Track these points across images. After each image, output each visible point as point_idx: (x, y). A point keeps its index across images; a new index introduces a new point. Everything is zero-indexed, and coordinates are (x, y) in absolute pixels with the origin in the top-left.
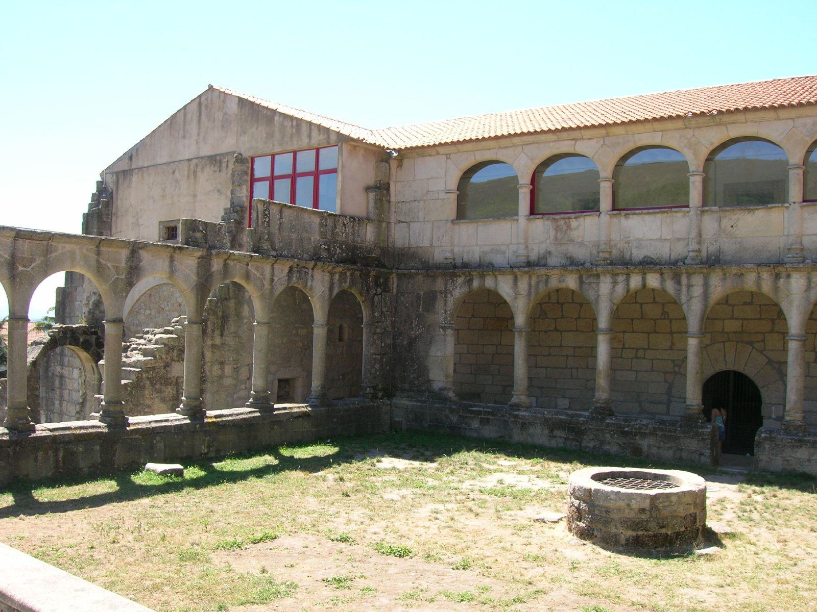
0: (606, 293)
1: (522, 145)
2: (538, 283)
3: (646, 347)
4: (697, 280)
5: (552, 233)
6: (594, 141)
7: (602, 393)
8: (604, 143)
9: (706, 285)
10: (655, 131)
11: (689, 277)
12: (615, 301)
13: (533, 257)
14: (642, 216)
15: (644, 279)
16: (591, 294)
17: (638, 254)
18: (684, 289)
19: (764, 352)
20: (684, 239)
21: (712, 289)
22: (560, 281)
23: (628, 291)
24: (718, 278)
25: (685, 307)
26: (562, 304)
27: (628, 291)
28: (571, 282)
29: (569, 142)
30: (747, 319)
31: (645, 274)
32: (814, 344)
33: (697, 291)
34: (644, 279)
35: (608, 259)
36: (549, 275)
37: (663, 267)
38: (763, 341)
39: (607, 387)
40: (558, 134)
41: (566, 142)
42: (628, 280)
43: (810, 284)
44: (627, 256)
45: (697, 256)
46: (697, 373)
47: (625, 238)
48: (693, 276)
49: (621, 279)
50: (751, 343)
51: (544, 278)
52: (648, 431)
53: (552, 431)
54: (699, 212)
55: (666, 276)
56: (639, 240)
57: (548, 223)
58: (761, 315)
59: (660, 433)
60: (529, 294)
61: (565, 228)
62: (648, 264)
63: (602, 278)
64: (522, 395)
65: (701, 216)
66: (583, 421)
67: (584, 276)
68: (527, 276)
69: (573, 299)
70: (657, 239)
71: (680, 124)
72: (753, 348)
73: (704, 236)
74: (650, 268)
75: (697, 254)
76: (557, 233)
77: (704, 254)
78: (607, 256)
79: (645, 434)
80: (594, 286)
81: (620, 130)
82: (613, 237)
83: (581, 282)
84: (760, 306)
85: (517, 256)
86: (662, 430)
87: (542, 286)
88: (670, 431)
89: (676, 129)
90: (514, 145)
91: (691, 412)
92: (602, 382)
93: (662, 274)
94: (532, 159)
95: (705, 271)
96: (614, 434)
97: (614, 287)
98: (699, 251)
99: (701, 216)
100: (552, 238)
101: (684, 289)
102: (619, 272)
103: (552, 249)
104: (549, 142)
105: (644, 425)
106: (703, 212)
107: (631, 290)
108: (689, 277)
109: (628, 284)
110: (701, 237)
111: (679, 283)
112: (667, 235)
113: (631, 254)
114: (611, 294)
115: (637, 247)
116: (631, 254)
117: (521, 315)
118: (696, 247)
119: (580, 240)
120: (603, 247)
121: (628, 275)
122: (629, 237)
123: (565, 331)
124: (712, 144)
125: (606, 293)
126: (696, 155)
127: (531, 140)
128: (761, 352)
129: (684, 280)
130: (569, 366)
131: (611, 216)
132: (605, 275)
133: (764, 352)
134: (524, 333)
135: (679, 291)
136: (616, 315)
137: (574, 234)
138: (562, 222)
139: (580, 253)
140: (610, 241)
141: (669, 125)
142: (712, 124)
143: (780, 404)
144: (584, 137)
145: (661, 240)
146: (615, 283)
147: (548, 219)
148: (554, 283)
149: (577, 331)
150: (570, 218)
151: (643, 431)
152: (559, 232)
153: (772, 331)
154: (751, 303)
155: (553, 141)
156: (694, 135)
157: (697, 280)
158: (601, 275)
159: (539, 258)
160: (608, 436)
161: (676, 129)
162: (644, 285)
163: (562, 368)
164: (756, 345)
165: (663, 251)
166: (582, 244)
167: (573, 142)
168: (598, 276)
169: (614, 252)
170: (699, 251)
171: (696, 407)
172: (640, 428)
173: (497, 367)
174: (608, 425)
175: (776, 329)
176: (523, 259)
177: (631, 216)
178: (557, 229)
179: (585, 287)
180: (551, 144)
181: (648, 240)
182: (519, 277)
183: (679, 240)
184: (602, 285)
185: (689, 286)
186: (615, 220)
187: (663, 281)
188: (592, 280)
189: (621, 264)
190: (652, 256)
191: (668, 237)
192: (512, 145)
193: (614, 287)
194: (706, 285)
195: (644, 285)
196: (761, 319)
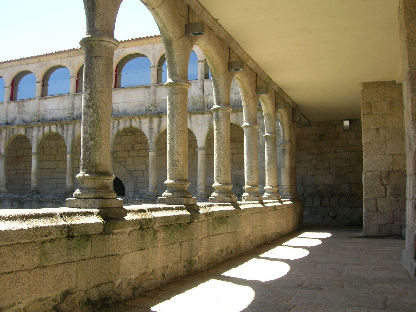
0: (36, 136)
1: (7, 68)
2: (9, 132)
3: (77, 167)
4: (70, 127)
5: (17, 109)
6: (34, 65)
7: (34, 185)
8: (38, 66)
9: (74, 129)
10: (58, 59)
11: (67, 127)
12: (39, 139)
13: (9, 121)
14: (52, 99)
15: (50, 128)
16: (29, 137)
17: (49, 117)
18: (65, 131)
19: (125, 166)
20: (67, 109)
21: (76, 131)
22: (18, 131)
23: (44, 134)
24: (78, 126)
25: (65, 140)
26: (44, 148)
27: (44, 134)
28: (22, 131)
29: (25, 65)
30: (119, 151)
31: (50, 125)
32: (146, 162)
33: (70, 132)
34: (50, 128)
35: (37, 119)
36: (14, 128)
37: (56, 121)
38: (125, 161)
39: (36, 181)
40: (19, 61)
41: (24, 66)
42: (44, 129)
43: (114, 126)
44: (45, 118)
45: (71, 116)
46: (70, 171)
47: (45, 109)
48: (69, 125)
49: (41, 128)
50: (120, 162)
51: (12, 130)
52: (49, 200)
53: (12, 203)
54: (73, 95)
55: (58, 126)
56: (50, 110)
57: (16, 104)
58: (124, 149)
59: (53, 201)
60: (6, 138)
61: (22, 106)
62: (53, 121)
63: (34, 128)
64: (3, 187)
65: (74, 97)
66: (24, 197)
67: (27, 128)
68: (5, 129)
69: (48, 146)
70: (57, 109)
71: (66, 55)
72: (121, 165)
73: (75, 107)
74: (51, 122)
75: (72, 115)
76: (19, 109)
77: (75, 115)
78: (37, 118)
79: (48, 201)
80: (31, 132)
81: (44, 59)
82: (40, 109)
83: (26, 131)
84: (124, 144)
85: (3, 120)
86: (54, 199)
87: (11, 134)
88: (58, 200)
89: (66, 57)
90: (4, 68)
91: (67, 190)
92: (33, 178)
93: (57, 125)
94: (10, 74)
95: (73, 122)
96: (36, 203)
97: (38, 133)
98: (72, 114)
99: (74, 97)
100: (17, 111)
101: (65, 131)
102: (40, 125)
103: (17, 116)
104: (17, 66)
105: (48, 198)
106: (75, 95)
107: (45, 133)
108: (67, 127)
109: (44, 131)
110: (74, 107)
111: (63, 129)
112: (61, 107)
113: (47, 117)
114: (37, 136)
115: (50, 113)
116: (47, 117)
117: (3, 149)
118: (71, 111)
119: (27, 112)
120: (36, 114)
121: (44, 126)
122: (46, 109)
123: (45, 161)
124: (79, 63)
125: (36, 136)
126: (73, 69)
127: (10, 65)
128: (124, 166)
129: (65, 128)
130: (46, 178)
131: (40, 99)
132: (35, 127)
133: (125, 166)
134: (4, 157)
135: (63, 133)
136: (41, 147)
137: (26, 109)
138: (21, 103)
139: (27, 118)
140: (39, 111)
141: (62, 55)
142: (80, 54)
143: (132, 191)
144: (31, 63)
145: (59, 109)
146: (39, 131)
147: (15, 102)
148: (16, 132)
149: (49, 160)
150: (24, 101)
151: (47, 200)
152: (20, 108)
153: (129, 156)
154: (120, 144)
155: (18, 65)
156: (73, 60)
157: (70, 127)
158: (34, 127)
159: (12, 121)
160: (34, 203)
161: (66, 57)
162: (50, 131)
163: (43, 179)
164: (122, 163)
165: (59, 114)
166: (28, 113)
167: (27, 65)
168: (32, 128)
169: (41, 116)
170: (72, 114)
171: (69, 188)
172: (46, 199)
173: (17, 180)
174: (34, 199)
175: (130, 155)
176: (5, 122)
177: (47, 99)
178: (19, 107)
179: (28, 133)
180: (18, 67)
181: (54, 110)
182: (2, 130)
183: (65, 109)
184: (34, 132)
185: (67, 130)
186: (41, 101)
187: (57, 128)
188: (30, 130)
189: (41, 121)
190: (55, 117)
191: (61, 108)
192: (2, 67)
193: (38, 133)
194: (74, 129)
195: (50, 131)
196: (124, 151)
